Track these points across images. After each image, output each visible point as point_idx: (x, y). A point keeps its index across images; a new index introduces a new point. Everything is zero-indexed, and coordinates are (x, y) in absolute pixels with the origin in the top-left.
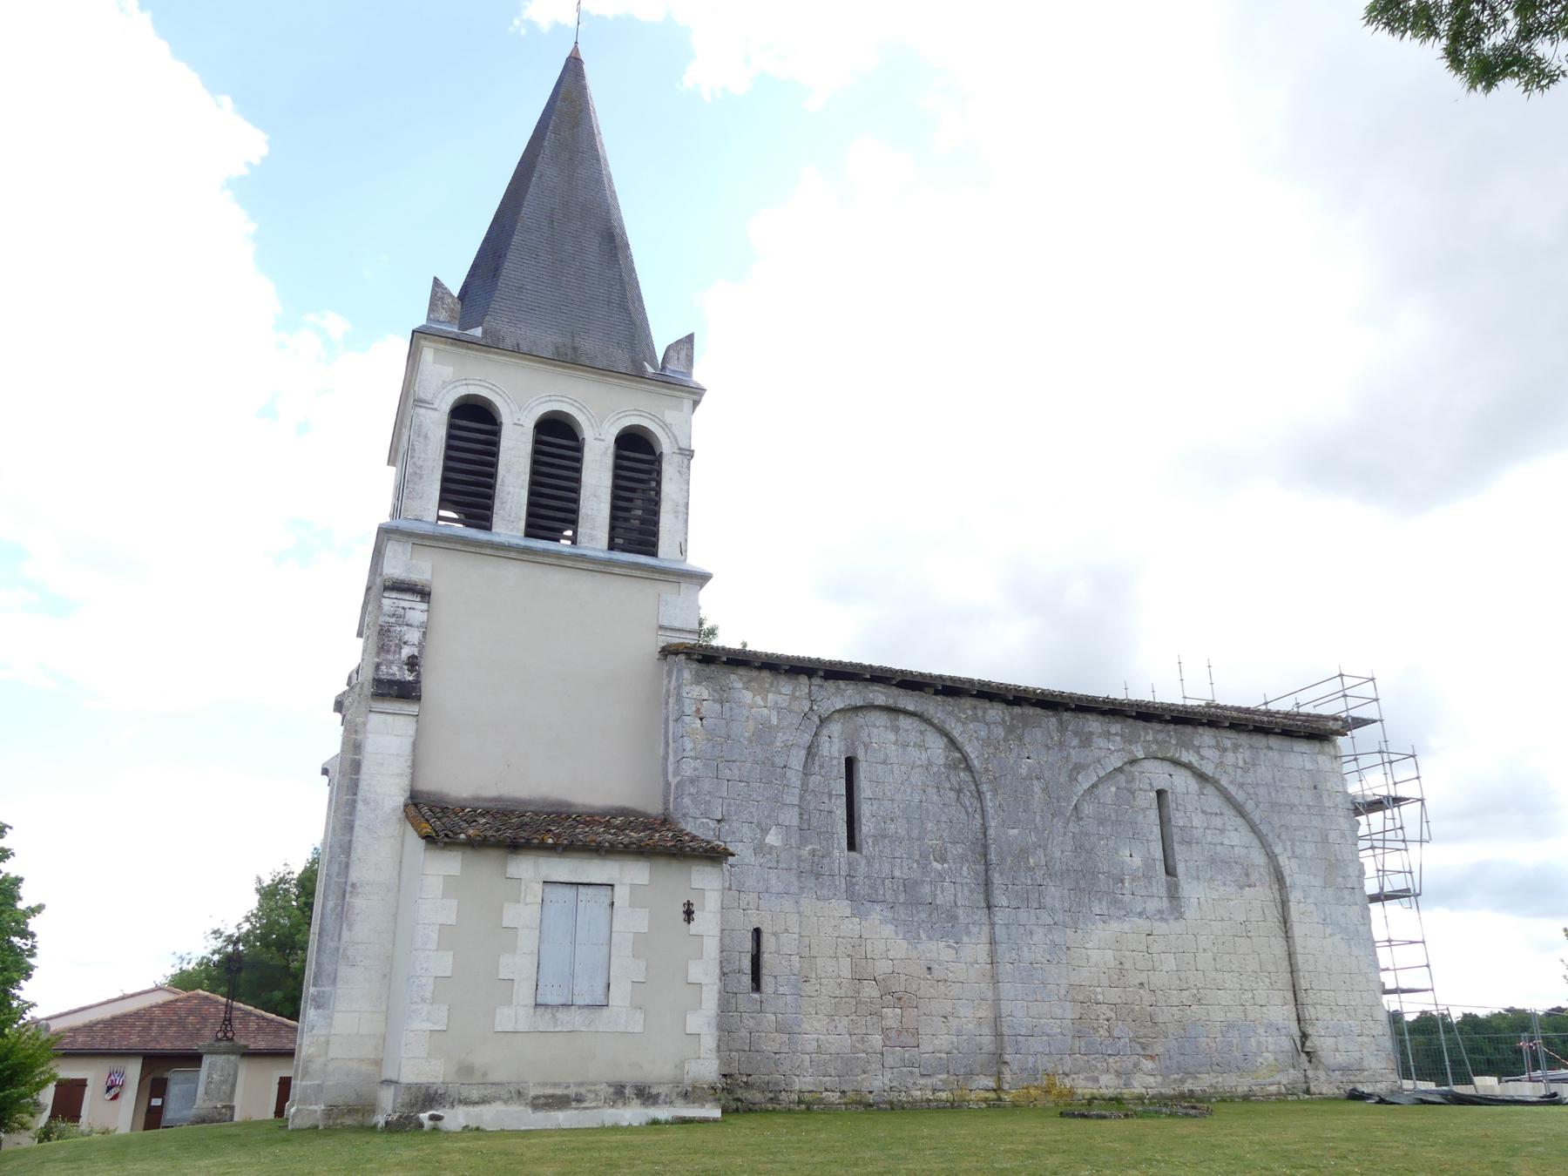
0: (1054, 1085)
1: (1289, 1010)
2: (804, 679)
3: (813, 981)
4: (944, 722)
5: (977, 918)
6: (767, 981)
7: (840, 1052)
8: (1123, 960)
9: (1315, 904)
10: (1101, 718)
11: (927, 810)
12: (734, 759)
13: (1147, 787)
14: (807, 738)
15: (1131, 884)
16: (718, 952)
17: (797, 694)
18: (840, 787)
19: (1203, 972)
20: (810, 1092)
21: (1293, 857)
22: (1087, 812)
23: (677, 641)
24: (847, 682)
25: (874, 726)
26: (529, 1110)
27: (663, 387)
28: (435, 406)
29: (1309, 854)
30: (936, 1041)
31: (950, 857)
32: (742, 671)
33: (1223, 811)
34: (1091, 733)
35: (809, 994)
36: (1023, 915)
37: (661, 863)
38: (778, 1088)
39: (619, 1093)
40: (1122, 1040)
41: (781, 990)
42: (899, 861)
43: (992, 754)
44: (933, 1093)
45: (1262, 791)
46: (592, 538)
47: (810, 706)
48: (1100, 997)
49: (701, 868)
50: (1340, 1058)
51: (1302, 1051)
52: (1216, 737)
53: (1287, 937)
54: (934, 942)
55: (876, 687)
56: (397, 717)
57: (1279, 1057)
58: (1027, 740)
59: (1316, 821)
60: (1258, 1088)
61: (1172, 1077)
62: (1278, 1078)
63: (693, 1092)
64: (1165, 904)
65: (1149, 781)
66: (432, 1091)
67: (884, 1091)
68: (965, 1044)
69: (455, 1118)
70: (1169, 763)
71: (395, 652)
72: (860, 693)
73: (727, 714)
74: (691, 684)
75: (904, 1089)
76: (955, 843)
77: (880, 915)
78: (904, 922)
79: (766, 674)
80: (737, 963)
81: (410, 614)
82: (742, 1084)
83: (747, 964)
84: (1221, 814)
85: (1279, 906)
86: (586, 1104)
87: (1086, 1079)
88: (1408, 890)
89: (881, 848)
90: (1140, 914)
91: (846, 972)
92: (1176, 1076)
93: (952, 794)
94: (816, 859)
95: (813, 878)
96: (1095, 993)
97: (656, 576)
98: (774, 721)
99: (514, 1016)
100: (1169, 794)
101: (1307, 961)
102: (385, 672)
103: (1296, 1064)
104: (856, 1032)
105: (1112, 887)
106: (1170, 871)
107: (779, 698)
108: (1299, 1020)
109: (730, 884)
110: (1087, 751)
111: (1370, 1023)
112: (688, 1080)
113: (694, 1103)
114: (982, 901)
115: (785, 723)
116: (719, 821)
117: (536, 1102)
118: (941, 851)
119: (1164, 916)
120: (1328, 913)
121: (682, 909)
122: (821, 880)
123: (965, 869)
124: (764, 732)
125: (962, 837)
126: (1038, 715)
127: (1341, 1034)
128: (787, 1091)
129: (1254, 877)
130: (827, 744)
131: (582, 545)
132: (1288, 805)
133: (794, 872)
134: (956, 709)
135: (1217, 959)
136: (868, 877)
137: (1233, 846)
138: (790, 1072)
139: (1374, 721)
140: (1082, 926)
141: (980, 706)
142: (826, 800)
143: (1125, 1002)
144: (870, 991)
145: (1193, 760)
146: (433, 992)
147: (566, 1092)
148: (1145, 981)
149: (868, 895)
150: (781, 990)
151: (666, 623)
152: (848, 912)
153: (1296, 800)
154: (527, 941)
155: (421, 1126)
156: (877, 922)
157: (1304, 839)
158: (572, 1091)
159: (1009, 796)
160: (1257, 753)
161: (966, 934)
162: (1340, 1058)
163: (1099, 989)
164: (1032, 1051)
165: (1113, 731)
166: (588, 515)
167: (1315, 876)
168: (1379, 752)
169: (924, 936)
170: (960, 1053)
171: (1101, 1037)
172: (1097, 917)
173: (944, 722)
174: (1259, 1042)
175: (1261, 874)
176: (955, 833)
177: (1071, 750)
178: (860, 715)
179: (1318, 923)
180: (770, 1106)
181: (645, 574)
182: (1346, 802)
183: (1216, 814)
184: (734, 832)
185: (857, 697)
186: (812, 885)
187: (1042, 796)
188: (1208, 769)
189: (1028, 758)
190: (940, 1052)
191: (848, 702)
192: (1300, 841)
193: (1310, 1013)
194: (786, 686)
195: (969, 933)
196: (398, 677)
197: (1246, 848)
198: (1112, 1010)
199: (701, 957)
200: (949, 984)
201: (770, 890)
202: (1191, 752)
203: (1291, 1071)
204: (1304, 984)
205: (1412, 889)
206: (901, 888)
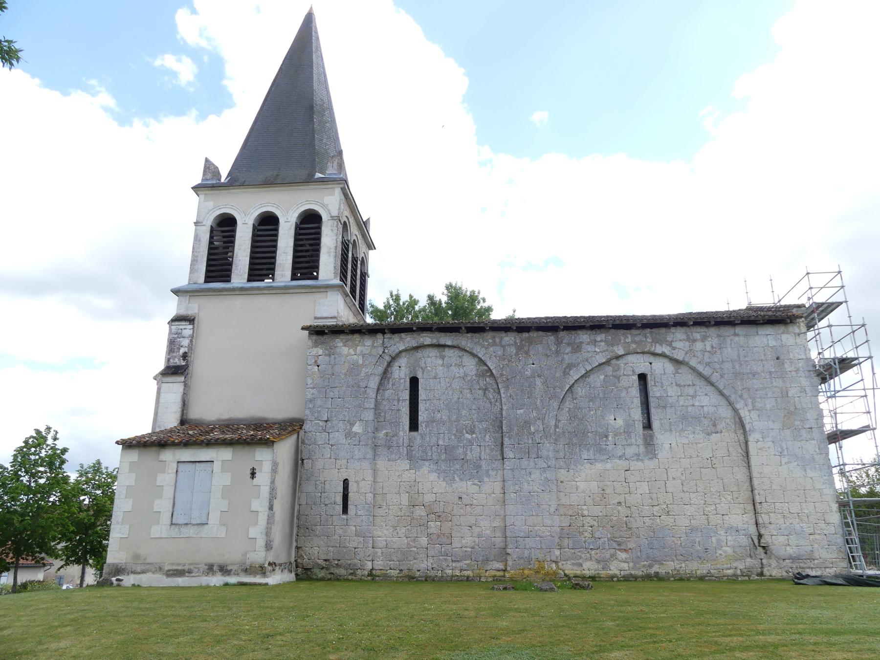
0: (543, 568)
1: (749, 518)
2: (380, 336)
4: (472, 349)
5: (494, 466)
6: (351, 507)
7: (400, 547)
8: (605, 488)
9: (773, 442)
10: (589, 332)
11: (463, 403)
12: (335, 386)
13: (631, 373)
14: (381, 369)
15: (614, 437)
16: (268, 494)
17: (375, 345)
18: (406, 395)
19: (672, 493)
20: (380, 570)
21: (753, 410)
22: (580, 394)
23: (321, 324)
25: (429, 357)
26: (165, 577)
27: (323, 185)
28: (204, 224)
29: (768, 407)
30: (464, 540)
31: (477, 430)
32: (342, 337)
33: (694, 383)
34: (581, 343)
35: (382, 515)
36: (524, 463)
37: (239, 448)
38: (356, 568)
39: (210, 569)
40: (602, 540)
42: (442, 435)
44: (461, 572)
45: (727, 366)
46: (282, 276)
47: (383, 350)
48: (586, 513)
49: (261, 449)
50: (791, 551)
51: (759, 546)
52: (686, 333)
53: (749, 466)
54: (465, 482)
55: (425, 334)
56: (175, 384)
57: (737, 550)
58: (531, 353)
59: (778, 383)
60: (716, 571)
61: (642, 563)
62: (735, 565)
63: (250, 569)
64: (642, 449)
65: (632, 369)
66: (119, 567)
68: (484, 542)
69: (128, 580)
70: (649, 355)
71: (177, 352)
72: (414, 339)
73: (332, 362)
74: (312, 348)
75: (441, 569)
76: (481, 421)
78: (444, 471)
79: (357, 337)
80: (333, 499)
81: (184, 331)
82: (334, 565)
83: (339, 499)
84: (694, 385)
85: (743, 446)
86: (193, 575)
87: (573, 564)
88: (868, 426)
90: (620, 457)
91: (405, 502)
92: (645, 563)
93: (481, 392)
94: (388, 438)
95: (386, 449)
96: (582, 509)
97: (313, 290)
98: (361, 362)
99: (160, 530)
100: (649, 376)
101: (763, 482)
102: (172, 362)
103: (752, 554)
105: (598, 441)
106: (648, 426)
107: (363, 348)
108: (757, 524)
109: (331, 456)
110: (578, 355)
111: (823, 525)
112: (248, 563)
113: (250, 574)
114: (499, 456)
115: (367, 362)
116: (326, 421)
117: (168, 573)
118: (471, 427)
119: (640, 458)
120: (785, 447)
121: (249, 472)
124: (354, 369)
125: (487, 418)
126: (540, 336)
127: (792, 533)
129: (720, 427)
130: (398, 371)
131: (277, 280)
132: (751, 373)
133: (369, 446)
135: (685, 484)
136: (422, 446)
137: (703, 407)
139: (841, 303)
140: (573, 467)
142: (396, 404)
143: (605, 514)
144: (420, 512)
145: (666, 351)
146: (123, 519)
147: (183, 568)
148: (622, 500)
149: (421, 456)
150: (359, 513)
151: (319, 315)
152: (408, 467)
153: (759, 369)
154: (168, 492)
155: (112, 583)
156: (426, 472)
157: (766, 396)
158: (186, 568)
160: (724, 339)
161: (487, 477)
162: (791, 551)
163: (585, 507)
164: (527, 546)
165: (598, 339)
166: (280, 264)
167: (774, 422)
168: (828, 326)
169: (457, 479)
171: (585, 538)
172: (586, 461)
173: (472, 349)
174: (719, 541)
175: (728, 424)
176: (482, 415)
177: (565, 356)
178: (419, 351)
179: (775, 455)
180: (350, 577)
181: (307, 290)
182: (808, 366)
183: (689, 385)
184: (333, 427)
185: (413, 341)
187: (542, 387)
188: (680, 356)
189: (533, 364)
190: (466, 547)
191: (408, 345)
192: (760, 398)
193: (763, 519)
194: (368, 341)
195: (488, 476)
196: (178, 364)
197: (716, 406)
198: (595, 520)
199: (259, 498)
200: (473, 507)
201: (354, 458)
202: (664, 345)
203: (749, 560)
204: (758, 499)
205: (871, 425)
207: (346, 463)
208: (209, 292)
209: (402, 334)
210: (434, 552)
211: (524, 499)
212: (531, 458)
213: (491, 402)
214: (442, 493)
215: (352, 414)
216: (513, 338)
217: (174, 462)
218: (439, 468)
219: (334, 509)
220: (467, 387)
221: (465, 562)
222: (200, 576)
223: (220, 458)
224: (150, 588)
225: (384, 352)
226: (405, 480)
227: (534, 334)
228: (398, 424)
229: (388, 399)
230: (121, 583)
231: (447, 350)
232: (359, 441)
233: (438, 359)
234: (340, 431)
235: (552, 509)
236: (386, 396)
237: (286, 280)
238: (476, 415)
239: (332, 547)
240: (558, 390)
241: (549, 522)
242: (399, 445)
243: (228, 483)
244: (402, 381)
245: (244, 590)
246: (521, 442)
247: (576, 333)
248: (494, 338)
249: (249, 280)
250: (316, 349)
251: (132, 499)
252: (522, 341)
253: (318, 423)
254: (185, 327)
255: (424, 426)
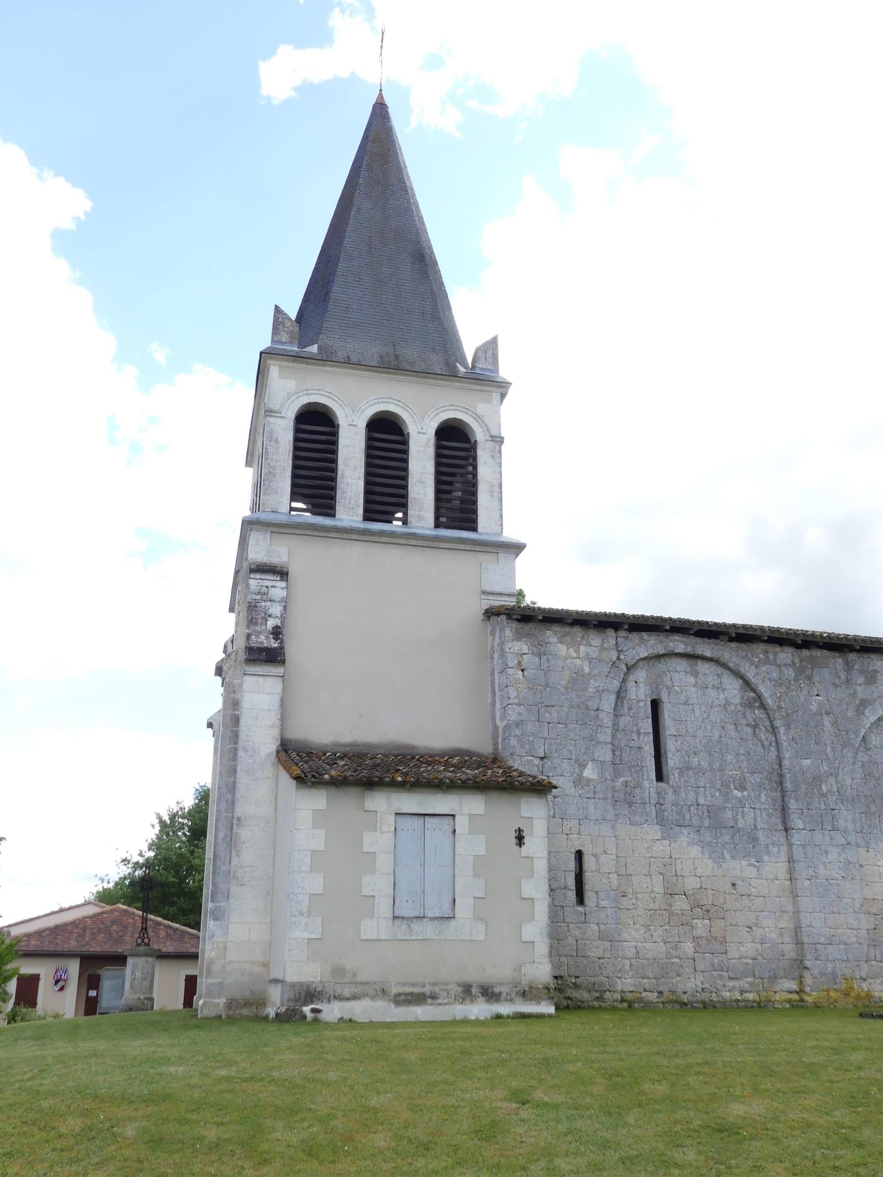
0: (852, 988)
2: (611, 633)
3: (630, 896)
5: (775, 839)
6: (589, 895)
7: (657, 957)
14: (616, 684)
17: (606, 645)
22: (874, 743)
24: (650, 633)
25: (676, 671)
28: (283, 415)
31: (748, 785)
32: (556, 628)
35: (627, 907)
37: (495, 797)
39: (467, 992)
41: (602, 904)
42: (702, 789)
43: (784, 692)
46: (420, 518)
54: (738, 861)
55: (676, 637)
56: (267, 679)
58: (816, 679)
63: (530, 991)
66: (312, 989)
67: (697, 992)
68: (769, 951)
69: (332, 1011)
72: (661, 642)
73: (545, 666)
74: (513, 640)
76: (753, 773)
77: (688, 837)
78: (709, 844)
79: (577, 630)
81: (272, 591)
82: (571, 985)
83: (571, 882)
86: (440, 1001)
89: (686, 779)
91: (659, 888)
93: (749, 730)
94: (628, 790)
95: (626, 807)
97: (477, 548)
98: (587, 670)
104: (670, 940)
107: (590, 650)
109: (554, 813)
110: (872, 688)
112: (525, 981)
113: (531, 1000)
116: (542, 758)
121: (513, 835)
122: (633, 808)
123: (763, 796)
124: (578, 680)
126: (825, 656)
128: (610, 991)
130: (634, 689)
131: (412, 525)
134: (749, 653)
138: (612, 975)
141: (771, 650)
142: (635, 738)
144: (681, 904)
147: (422, 990)
149: (676, 820)
150: (602, 904)
151: (488, 589)
152: (659, 835)
154: (384, 863)
156: (685, 844)
158: (427, 990)
159: (801, 730)
161: (766, 854)
164: (831, 957)
166: (416, 499)
169: (727, 856)
170: (764, 959)
176: (753, 764)
177: (858, 688)
180: (596, 1004)
181: (467, 547)
185: (659, 646)
186: (626, 813)
191: (651, 651)
194: (595, 639)
195: (768, 853)
196: (265, 645)
206: (706, 814)
207: (578, 826)
208: (306, 529)
209: (643, 633)
210: (705, 965)
211: (821, 889)
212: (825, 830)
213: (763, 746)
214: (708, 876)
215: (580, 750)
216: (790, 656)
217: (390, 814)
218: (702, 839)
219: (565, 896)
220: (730, 720)
221: (747, 980)
222: (451, 1004)
223: (466, 811)
224: (371, 1025)
225: (618, 658)
226: (658, 854)
227: (817, 653)
228: (640, 769)
229: (623, 730)
230: (319, 1016)
231: (700, 662)
232: (595, 793)
233: (689, 676)
234: (565, 774)
235: (857, 905)
236: (621, 726)
237: (426, 526)
238: (745, 763)
239: (566, 956)
240: (853, 736)
241: (855, 924)
242: (644, 802)
243: (482, 852)
244: (642, 704)
245: (521, 1027)
246: (811, 807)
247: (869, 658)
248: (767, 652)
249: (366, 518)
250: (519, 643)
251: (322, 874)
252: (801, 661)
253: (532, 761)
254: (274, 583)
255: (676, 773)
